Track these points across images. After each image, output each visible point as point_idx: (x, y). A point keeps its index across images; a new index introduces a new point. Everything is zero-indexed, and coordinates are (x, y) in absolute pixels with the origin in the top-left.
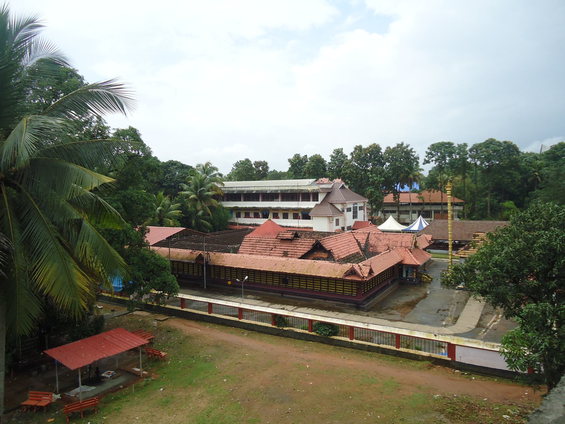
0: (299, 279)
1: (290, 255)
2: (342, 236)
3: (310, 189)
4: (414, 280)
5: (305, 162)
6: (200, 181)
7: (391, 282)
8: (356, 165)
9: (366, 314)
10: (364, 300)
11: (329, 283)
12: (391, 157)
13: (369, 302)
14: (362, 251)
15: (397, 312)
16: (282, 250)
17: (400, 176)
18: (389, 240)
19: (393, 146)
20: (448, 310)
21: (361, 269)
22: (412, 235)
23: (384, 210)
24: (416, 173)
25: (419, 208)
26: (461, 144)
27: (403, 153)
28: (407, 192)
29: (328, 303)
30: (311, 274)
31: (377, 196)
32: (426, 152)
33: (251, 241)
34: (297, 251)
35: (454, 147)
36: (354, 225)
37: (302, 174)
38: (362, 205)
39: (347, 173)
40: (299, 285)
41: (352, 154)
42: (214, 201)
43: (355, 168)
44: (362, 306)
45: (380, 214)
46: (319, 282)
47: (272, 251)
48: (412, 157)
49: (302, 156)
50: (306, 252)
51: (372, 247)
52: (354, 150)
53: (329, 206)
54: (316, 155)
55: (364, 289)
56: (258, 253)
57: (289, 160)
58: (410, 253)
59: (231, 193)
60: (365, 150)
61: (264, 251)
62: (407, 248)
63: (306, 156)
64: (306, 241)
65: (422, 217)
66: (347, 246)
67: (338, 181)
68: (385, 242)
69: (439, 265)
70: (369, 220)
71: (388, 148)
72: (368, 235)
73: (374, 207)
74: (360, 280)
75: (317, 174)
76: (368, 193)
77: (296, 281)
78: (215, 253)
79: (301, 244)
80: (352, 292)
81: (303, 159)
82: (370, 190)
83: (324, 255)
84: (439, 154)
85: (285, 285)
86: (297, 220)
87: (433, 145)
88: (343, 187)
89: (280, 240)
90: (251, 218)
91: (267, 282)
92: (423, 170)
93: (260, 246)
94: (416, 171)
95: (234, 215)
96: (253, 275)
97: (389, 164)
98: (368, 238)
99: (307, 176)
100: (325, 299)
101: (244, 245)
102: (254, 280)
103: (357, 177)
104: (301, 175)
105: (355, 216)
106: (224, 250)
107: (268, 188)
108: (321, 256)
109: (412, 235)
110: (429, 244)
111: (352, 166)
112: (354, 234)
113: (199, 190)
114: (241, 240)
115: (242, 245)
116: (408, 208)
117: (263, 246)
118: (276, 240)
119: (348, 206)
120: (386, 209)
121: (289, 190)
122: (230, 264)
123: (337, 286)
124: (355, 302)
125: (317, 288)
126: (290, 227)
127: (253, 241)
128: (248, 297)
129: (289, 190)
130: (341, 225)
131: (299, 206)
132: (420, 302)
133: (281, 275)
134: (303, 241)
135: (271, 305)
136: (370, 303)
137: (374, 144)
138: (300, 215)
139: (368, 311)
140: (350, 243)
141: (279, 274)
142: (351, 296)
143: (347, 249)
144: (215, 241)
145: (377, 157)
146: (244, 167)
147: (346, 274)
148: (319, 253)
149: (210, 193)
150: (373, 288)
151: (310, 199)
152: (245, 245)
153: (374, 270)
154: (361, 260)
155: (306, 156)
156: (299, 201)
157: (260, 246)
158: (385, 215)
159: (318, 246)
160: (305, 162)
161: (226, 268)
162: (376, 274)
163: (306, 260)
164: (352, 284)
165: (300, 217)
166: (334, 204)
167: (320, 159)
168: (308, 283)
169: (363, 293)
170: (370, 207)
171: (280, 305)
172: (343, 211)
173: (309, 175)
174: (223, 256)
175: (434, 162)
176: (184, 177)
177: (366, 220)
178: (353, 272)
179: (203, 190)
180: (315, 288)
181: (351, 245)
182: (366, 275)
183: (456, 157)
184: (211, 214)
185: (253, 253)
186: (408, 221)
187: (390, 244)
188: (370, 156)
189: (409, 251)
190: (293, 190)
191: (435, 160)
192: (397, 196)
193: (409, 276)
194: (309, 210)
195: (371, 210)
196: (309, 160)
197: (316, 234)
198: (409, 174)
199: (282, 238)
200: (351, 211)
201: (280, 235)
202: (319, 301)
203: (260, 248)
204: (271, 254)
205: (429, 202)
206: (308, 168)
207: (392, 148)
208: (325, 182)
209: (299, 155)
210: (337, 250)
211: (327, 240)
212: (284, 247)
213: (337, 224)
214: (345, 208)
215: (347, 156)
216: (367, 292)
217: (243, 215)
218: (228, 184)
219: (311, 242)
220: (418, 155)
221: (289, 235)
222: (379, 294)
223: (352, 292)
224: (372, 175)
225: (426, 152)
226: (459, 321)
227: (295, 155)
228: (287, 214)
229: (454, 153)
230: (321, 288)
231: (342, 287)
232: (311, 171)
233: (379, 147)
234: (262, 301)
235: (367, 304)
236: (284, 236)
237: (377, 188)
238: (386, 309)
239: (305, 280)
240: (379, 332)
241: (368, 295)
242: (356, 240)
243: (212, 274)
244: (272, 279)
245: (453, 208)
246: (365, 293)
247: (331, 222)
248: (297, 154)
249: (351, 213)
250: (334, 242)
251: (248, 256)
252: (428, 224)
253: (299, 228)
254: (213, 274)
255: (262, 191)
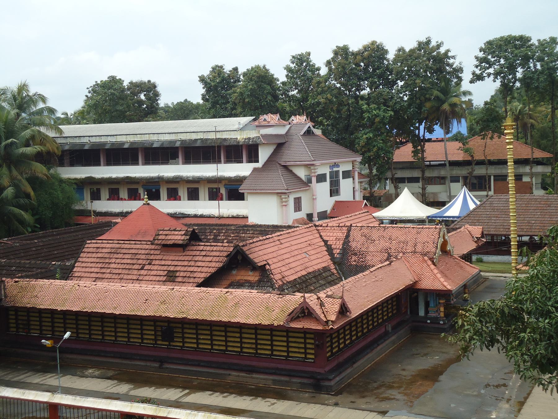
0: (197, 329)
1: (180, 279)
2: (293, 234)
3: (241, 137)
4: (442, 322)
5: (235, 82)
6: (5, 125)
7: (394, 328)
8: (338, 85)
9: (333, 400)
10: (332, 371)
11: (259, 337)
12: (406, 69)
13: (341, 373)
14: (334, 263)
15: (399, 393)
16: (165, 268)
17: (425, 106)
18: (390, 239)
19: (410, 45)
20: (504, 385)
21: (322, 305)
22: (436, 228)
23: (396, 176)
24: (455, 100)
25: (463, 172)
26: (545, 40)
27: (429, 61)
28: (438, 141)
29: (257, 378)
30: (220, 319)
31: (379, 149)
32: (477, 58)
33: (100, 250)
34: (196, 269)
35: (532, 45)
36: (333, 209)
37: (229, 106)
38: (349, 167)
39: (319, 103)
40: (198, 343)
41: (328, 63)
42: (40, 169)
43: (335, 92)
44: (327, 383)
45: (389, 187)
46: (238, 335)
47: (142, 272)
48: (447, 68)
49: (228, 69)
50: (213, 270)
51: (355, 254)
52: (332, 55)
53: (280, 171)
54: (258, 67)
55: (331, 346)
56: (114, 276)
57: (202, 79)
58: (432, 267)
59: (77, 148)
60: (355, 54)
61: (127, 272)
62: (425, 255)
63: (236, 69)
64: (215, 248)
65: (467, 190)
66: (304, 255)
67: (297, 119)
68: (384, 244)
69: (496, 288)
70: (365, 198)
71: (401, 50)
72: (349, 231)
73: (374, 171)
74: (320, 328)
75: (261, 106)
76: (362, 143)
77: (190, 334)
78: (17, 280)
79: (204, 253)
80: (306, 353)
81: (229, 76)
82: (364, 136)
83: (253, 277)
84: (502, 61)
85: (167, 343)
86: (215, 203)
87: (489, 43)
88: (309, 132)
89: (159, 247)
90: (122, 199)
91: (129, 338)
92: (470, 93)
93: (118, 261)
94: (455, 96)
95: (87, 195)
96: (126, 326)
97: (403, 82)
98: (348, 236)
99: (239, 110)
100: (251, 370)
101: (84, 260)
102: (103, 336)
103: (339, 111)
104: (226, 108)
105: (334, 191)
106: (41, 273)
107: (154, 138)
108: (246, 278)
109: (436, 228)
110: (476, 245)
111: (331, 88)
112: (319, 228)
113: (3, 144)
114: (76, 252)
115: (80, 259)
116: (443, 173)
117: (125, 261)
118: (153, 247)
119: (320, 171)
120: (400, 174)
121: (199, 141)
122: (48, 303)
123: (275, 343)
124: (311, 375)
125: (234, 347)
126: (202, 216)
127: (104, 250)
128: (86, 373)
129: (199, 141)
130: (306, 209)
131: (221, 174)
132: (448, 369)
133: (158, 323)
134: (208, 248)
135: (134, 389)
136: (343, 375)
137: (373, 43)
138: (223, 191)
139: (339, 393)
140: (309, 248)
141: (155, 321)
142: (303, 361)
143: (301, 262)
144: (31, 253)
145: (378, 68)
146: (105, 93)
147: (291, 316)
148: (243, 272)
149: (29, 150)
150: (352, 342)
151: (220, 158)
152: (87, 260)
153: (350, 306)
154: (332, 283)
155: (236, 69)
156: (220, 162)
157: (118, 261)
158: (396, 188)
159: (239, 258)
160: (235, 82)
161: (41, 311)
162: (355, 312)
163: (209, 289)
164: (305, 338)
165: (222, 195)
166: (291, 168)
167: (266, 76)
168: (214, 338)
169: (329, 354)
170: (366, 171)
171: (153, 388)
172: (310, 181)
173: (243, 108)
174: (34, 287)
175: (492, 77)
176: (251, 95)
177: (359, 197)
178: (306, 311)
179: (12, 143)
180: (275, 353)
181: (313, 252)
182: (333, 318)
183: (535, 66)
184: (32, 193)
185: (104, 276)
186: (442, 197)
187: (393, 248)
188: (366, 69)
189: (430, 263)
190: (207, 140)
191: (494, 74)
192: (419, 148)
193: (432, 314)
194: (240, 180)
195: (368, 177)
196: (242, 77)
197: (249, 230)
198: (443, 102)
199: (164, 242)
200: (325, 181)
201: (160, 237)
202: (238, 376)
203: (120, 266)
204: (141, 278)
205: (483, 158)
206: (241, 94)
207: (407, 50)
208: (272, 123)
209: (221, 67)
210: (279, 264)
211: (260, 243)
212: (169, 263)
213: (298, 207)
214: (313, 174)
215: (318, 69)
216: (337, 352)
217: (105, 193)
218: (69, 130)
219: (225, 249)
220: (460, 63)
221: (179, 237)
222: (364, 356)
223: (306, 353)
224: (369, 105)
225: (477, 58)
226: (526, 409)
227: (214, 69)
228: (99, 191)
229: (531, 58)
230: (242, 348)
231: (224, 339)
232: (247, 100)
233: (383, 49)
234: (116, 381)
235: (338, 379)
236: (169, 237)
237: (378, 131)
238: (377, 388)
239: (194, 331)
240: (30, 403)
241: (341, 359)
242: (324, 241)
243: (12, 325)
244: (139, 332)
245: (531, 169)
246: (333, 354)
247: (284, 204)
248: (217, 66)
249: (325, 186)
250: (276, 248)
251: (88, 283)
252: (478, 203)
253: (220, 217)
254: (15, 325)
255: (142, 143)
